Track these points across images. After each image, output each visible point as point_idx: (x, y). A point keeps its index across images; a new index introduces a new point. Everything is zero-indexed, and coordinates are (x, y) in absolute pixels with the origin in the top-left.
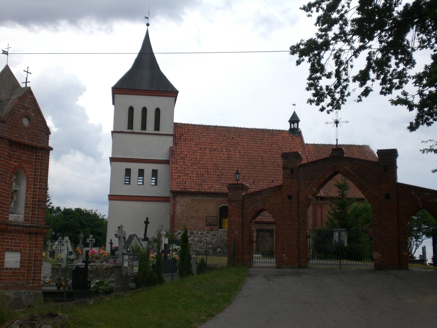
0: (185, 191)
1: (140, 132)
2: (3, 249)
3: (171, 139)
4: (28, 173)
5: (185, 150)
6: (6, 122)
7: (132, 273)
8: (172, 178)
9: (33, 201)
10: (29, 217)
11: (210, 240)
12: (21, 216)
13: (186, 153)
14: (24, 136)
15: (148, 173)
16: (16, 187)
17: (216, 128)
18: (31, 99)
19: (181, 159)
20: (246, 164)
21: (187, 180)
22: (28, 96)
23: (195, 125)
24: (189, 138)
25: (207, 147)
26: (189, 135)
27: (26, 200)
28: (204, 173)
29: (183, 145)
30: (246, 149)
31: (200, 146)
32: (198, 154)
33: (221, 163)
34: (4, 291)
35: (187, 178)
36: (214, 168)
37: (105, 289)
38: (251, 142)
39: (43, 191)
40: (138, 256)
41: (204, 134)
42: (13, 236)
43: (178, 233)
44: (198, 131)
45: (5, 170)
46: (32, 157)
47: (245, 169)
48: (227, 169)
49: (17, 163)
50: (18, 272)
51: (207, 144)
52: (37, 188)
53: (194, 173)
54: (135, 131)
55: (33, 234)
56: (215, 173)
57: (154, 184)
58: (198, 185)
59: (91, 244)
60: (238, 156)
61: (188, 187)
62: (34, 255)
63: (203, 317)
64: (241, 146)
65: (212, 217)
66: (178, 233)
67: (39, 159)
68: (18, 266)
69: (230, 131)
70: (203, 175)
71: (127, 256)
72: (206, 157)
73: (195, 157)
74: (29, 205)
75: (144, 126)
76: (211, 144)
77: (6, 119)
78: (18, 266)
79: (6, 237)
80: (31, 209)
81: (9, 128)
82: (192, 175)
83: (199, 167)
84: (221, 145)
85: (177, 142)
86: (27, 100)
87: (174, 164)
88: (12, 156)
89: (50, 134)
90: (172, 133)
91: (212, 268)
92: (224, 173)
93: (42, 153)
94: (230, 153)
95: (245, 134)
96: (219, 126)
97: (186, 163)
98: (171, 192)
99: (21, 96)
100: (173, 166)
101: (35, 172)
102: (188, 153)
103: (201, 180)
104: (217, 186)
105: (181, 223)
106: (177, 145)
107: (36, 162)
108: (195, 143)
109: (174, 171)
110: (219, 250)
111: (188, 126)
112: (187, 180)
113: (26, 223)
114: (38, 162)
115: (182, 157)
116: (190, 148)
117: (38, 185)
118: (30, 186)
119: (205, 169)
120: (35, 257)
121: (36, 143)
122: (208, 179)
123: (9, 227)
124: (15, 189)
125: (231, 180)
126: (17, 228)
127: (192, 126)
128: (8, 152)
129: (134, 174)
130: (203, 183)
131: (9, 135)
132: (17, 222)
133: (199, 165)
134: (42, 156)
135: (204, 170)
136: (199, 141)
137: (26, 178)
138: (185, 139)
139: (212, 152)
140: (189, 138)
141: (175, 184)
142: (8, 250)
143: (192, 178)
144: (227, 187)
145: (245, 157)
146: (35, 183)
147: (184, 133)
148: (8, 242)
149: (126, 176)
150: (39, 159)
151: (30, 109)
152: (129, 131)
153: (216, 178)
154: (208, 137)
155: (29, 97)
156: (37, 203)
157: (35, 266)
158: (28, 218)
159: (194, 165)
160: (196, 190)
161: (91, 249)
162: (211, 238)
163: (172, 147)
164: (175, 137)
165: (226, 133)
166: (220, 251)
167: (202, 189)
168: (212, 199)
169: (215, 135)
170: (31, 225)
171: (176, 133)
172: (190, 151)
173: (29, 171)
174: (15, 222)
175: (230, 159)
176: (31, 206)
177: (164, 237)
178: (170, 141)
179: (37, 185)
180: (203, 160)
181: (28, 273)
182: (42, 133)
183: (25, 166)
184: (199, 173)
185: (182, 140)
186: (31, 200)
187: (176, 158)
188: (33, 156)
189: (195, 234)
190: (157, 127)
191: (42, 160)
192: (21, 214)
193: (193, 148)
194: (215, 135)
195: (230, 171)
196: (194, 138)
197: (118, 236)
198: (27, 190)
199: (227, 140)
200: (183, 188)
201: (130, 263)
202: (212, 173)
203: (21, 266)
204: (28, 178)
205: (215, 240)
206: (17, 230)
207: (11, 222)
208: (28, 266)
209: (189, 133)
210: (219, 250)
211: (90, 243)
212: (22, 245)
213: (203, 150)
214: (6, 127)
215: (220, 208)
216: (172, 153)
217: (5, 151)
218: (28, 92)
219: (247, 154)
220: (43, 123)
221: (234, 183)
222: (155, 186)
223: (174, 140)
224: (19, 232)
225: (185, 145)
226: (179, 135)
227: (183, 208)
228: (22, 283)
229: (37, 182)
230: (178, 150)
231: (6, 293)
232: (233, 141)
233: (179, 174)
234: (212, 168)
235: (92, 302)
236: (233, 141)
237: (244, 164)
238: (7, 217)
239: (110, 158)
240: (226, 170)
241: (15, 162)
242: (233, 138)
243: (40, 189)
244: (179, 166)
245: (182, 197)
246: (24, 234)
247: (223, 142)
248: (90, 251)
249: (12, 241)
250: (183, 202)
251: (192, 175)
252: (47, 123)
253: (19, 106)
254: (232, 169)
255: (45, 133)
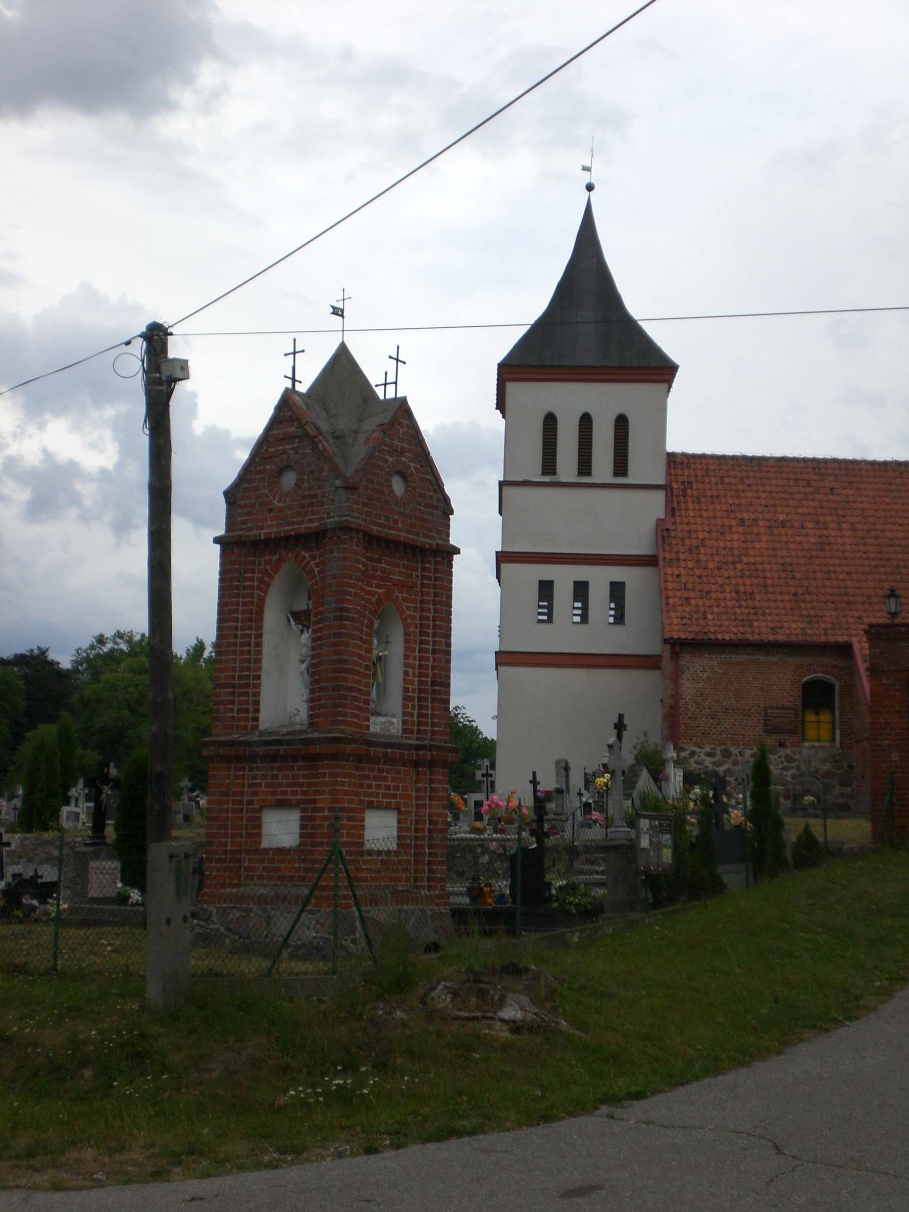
0: (705, 638)
1: (575, 481)
2: (361, 802)
3: (659, 498)
4: (407, 613)
5: (700, 528)
6: (356, 489)
7: (658, 866)
8: (667, 604)
9: (420, 682)
10: (413, 724)
11: (778, 771)
12: (394, 720)
13: (701, 536)
14: (396, 521)
15: (599, 595)
16: (381, 648)
17: (784, 464)
18: (408, 426)
19: (690, 550)
20: (873, 563)
21: (708, 610)
22: (402, 421)
23: (724, 458)
24: (708, 493)
25: (760, 516)
26: (708, 486)
27: (405, 681)
28: (756, 589)
29: (691, 514)
30: (871, 520)
31: (739, 515)
32: (735, 537)
33: (802, 561)
34: (369, 908)
35: (708, 603)
36: (783, 575)
37: (582, 903)
38: (886, 500)
39: (443, 657)
40: (670, 820)
41: (752, 481)
42: (380, 770)
43: (688, 752)
44: (732, 473)
45: (359, 608)
46: (414, 574)
47: (870, 577)
48: (819, 575)
49: (383, 590)
50: (394, 861)
51: (759, 509)
52: (427, 651)
53: (727, 588)
54: (563, 480)
55: (423, 766)
56: (785, 590)
57: (577, 619)
58: (741, 623)
59: (487, 782)
60: (848, 541)
61: (712, 629)
62: (429, 817)
63: (878, 983)
64: (856, 512)
65: (783, 708)
66: (688, 752)
67: (429, 578)
68: (393, 846)
69: (823, 470)
70: (752, 594)
71: (647, 821)
72: (757, 545)
73: (729, 544)
74: (411, 694)
75: (585, 466)
76: (771, 509)
77: (358, 481)
78: (393, 846)
79: (367, 773)
80: (416, 703)
81: (364, 505)
82: (721, 596)
83: (739, 574)
84: (800, 510)
85: (675, 505)
86: (401, 431)
87: (669, 567)
88: (371, 572)
89: (452, 513)
90: (661, 481)
91: (835, 852)
92: (810, 589)
93: (436, 563)
94: (825, 533)
95: (840, 470)
96: (791, 456)
97: (702, 564)
98: (666, 641)
99: (386, 421)
100: (669, 571)
101: (422, 610)
102: (706, 535)
103: (747, 608)
104: (794, 626)
105: (697, 727)
106: (677, 513)
107: (423, 585)
108: (724, 507)
109: (670, 586)
110: (809, 798)
111: (704, 461)
112: (708, 610)
113: (406, 738)
114: (429, 586)
115: (692, 545)
116: (713, 522)
117: (431, 643)
118: (411, 645)
119: (757, 577)
120: (431, 822)
121: (423, 537)
122: (766, 604)
123: (372, 749)
124: (380, 654)
125: (832, 606)
126: (389, 750)
127: (716, 461)
128: (364, 565)
129: (563, 594)
130: (753, 617)
131: (365, 521)
132: (389, 736)
133: (738, 566)
134: (436, 571)
135: (756, 581)
136: (737, 501)
137: (403, 626)
138: (699, 497)
139: (775, 531)
140: (708, 493)
141: (675, 621)
142: (371, 806)
143: (722, 604)
144: (866, 632)
145: (869, 541)
146: (424, 638)
147: (693, 479)
148: (370, 786)
149: (541, 599)
150: (429, 578)
151: (408, 454)
152: (547, 479)
153: (790, 601)
154: (761, 488)
155: (405, 422)
156: (429, 688)
157: (431, 846)
158: (410, 727)
159: (724, 566)
160: (733, 637)
161: (488, 797)
162: (781, 766)
163: (662, 520)
164: (669, 490)
165: (813, 477)
166: (811, 804)
167: (752, 633)
168: (781, 662)
169: (781, 482)
170: (419, 743)
171: (671, 481)
172: (714, 529)
173: (408, 608)
174: (384, 736)
175: (827, 547)
176: (416, 695)
177: (674, 767)
178: (656, 504)
179: (427, 643)
180: (751, 552)
181: (416, 863)
182: (434, 511)
183: (400, 595)
184: (742, 589)
185: (689, 499)
186: (416, 679)
187: (675, 549)
188: (416, 570)
189: (736, 755)
190: (621, 466)
191: (436, 579)
192: (394, 716)
193: (720, 522)
194: (781, 482)
195: (827, 582)
196: (721, 493)
197: (611, 768)
198: (406, 657)
199: (817, 497)
200: (700, 631)
201: (654, 840)
202: (778, 589)
203: (399, 845)
204: (406, 626)
205: (791, 772)
206: (389, 756)
207: (375, 735)
208: (416, 846)
209: (707, 480)
210: (809, 798)
211: (484, 781)
212: (400, 792)
213: (748, 526)
214: (356, 502)
215: (803, 685)
216: (663, 537)
217: (357, 561)
218: (402, 407)
219: (873, 534)
220: (436, 487)
221: (881, 621)
222: (583, 626)
223: (669, 501)
224: (284, 758)
225: (698, 513)
226: (682, 487)
227: (701, 685)
228: (404, 888)
229: (427, 634)
230: (679, 527)
231: (372, 912)
232: (832, 498)
233: (685, 594)
234: (776, 575)
235: (577, 938)
236: (832, 498)
237: (866, 562)
238: (365, 723)
239: (497, 552)
240: (815, 579)
241: (378, 586)
242: (832, 489)
243: (434, 652)
244: (683, 572)
245: (696, 657)
246: (404, 764)
247: (805, 503)
248: (485, 803)
249: (380, 783)
250: (701, 669)
251: (721, 596)
252: (445, 487)
253: (384, 447)
254: (833, 576)
255: (441, 513)
